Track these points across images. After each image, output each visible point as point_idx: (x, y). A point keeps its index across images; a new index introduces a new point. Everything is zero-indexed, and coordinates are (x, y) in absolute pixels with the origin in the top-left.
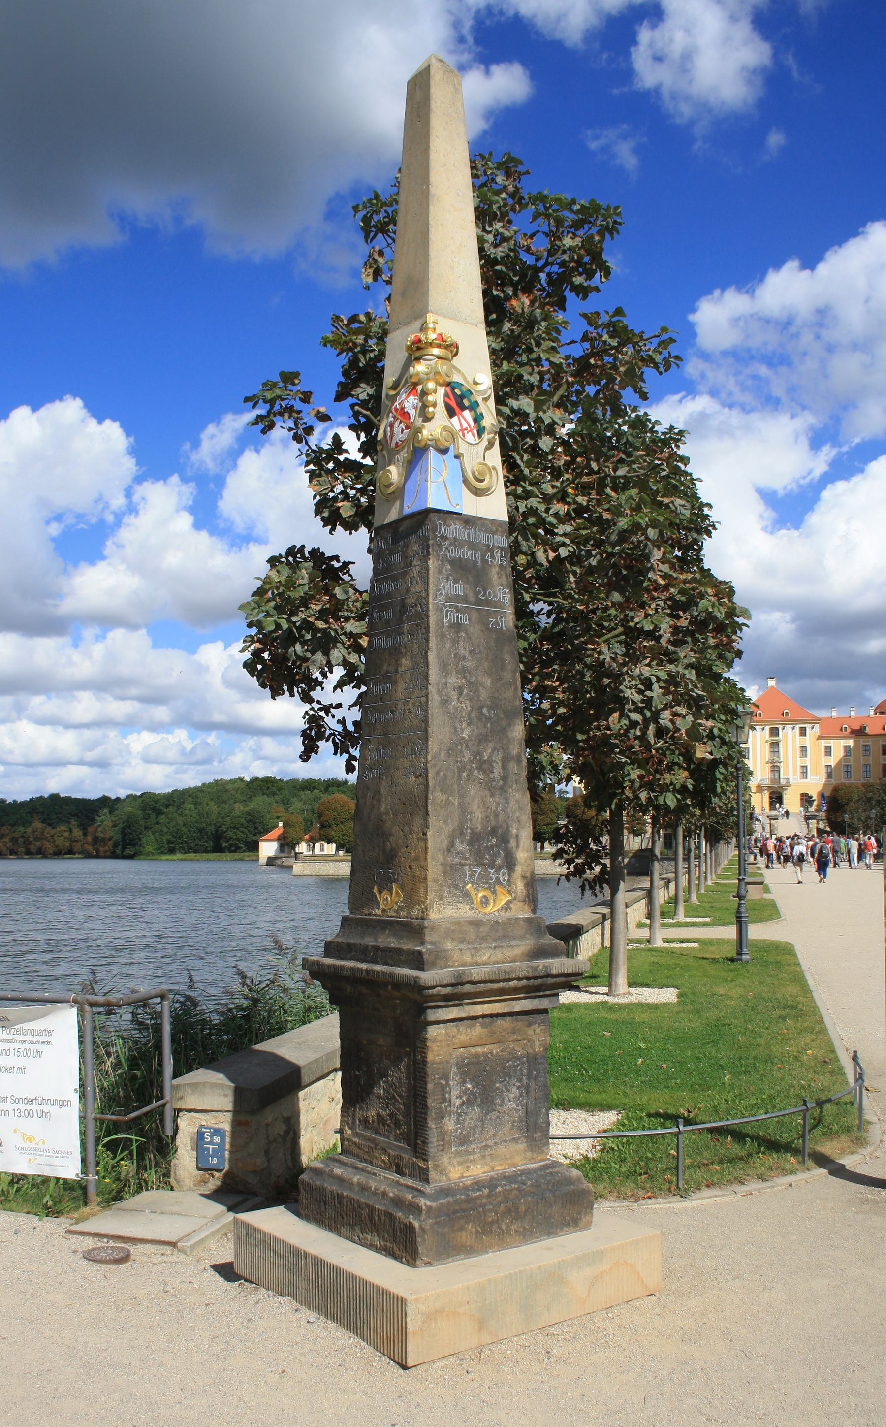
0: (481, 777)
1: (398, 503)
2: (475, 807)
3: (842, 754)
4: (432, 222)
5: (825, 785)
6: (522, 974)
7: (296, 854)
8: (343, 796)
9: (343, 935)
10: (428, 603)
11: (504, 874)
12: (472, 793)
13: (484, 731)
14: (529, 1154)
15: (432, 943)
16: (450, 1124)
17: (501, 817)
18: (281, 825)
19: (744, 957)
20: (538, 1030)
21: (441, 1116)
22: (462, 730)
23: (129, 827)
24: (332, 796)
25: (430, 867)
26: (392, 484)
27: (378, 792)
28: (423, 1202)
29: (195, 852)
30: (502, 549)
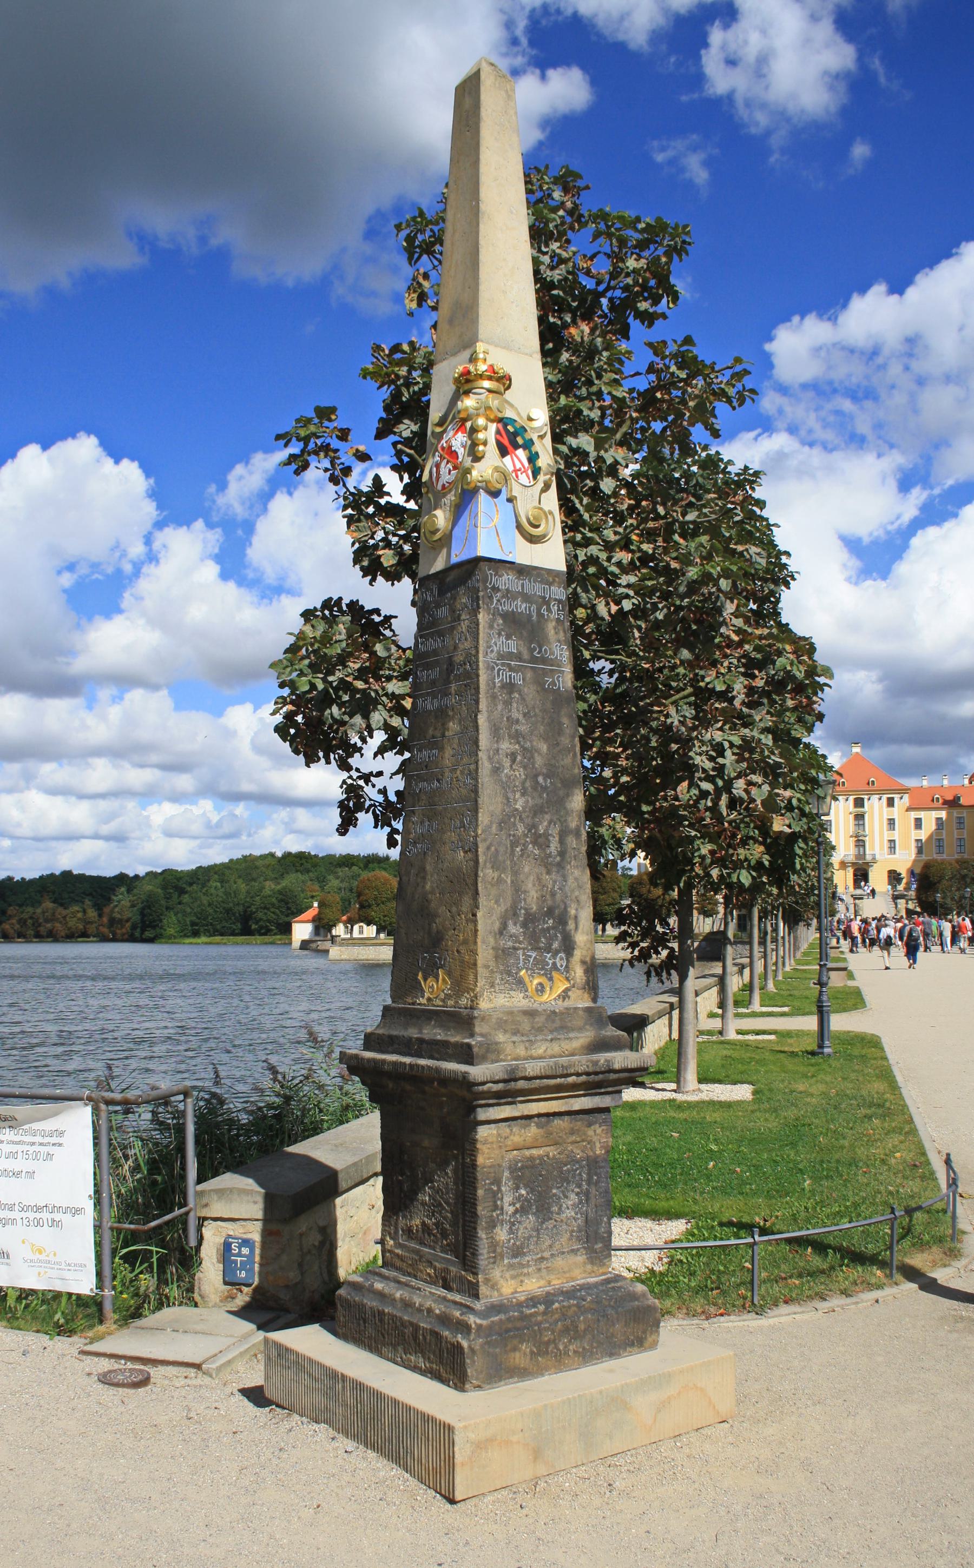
0: (537, 852)
1: (445, 551)
2: (530, 885)
3: (934, 827)
4: (482, 242)
5: (915, 861)
6: (581, 1069)
7: (333, 937)
8: (384, 873)
9: (384, 1027)
10: (478, 661)
11: (561, 959)
12: (526, 869)
13: (539, 801)
14: (589, 1267)
15: (482, 1035)
16: (502, 1234)
17: (558, 897)
18: (316, 904)
19: (826, 1050)
20: (599, 1131)
21: (492, 1224)
22: (516, 801)
23: (149, 907)
24: (372, 873)
25: (480, 951)
26: (438, 530)
27: (423, 869)
28: (472, 1320)
29: (222, 935)
30: (560, 601)
